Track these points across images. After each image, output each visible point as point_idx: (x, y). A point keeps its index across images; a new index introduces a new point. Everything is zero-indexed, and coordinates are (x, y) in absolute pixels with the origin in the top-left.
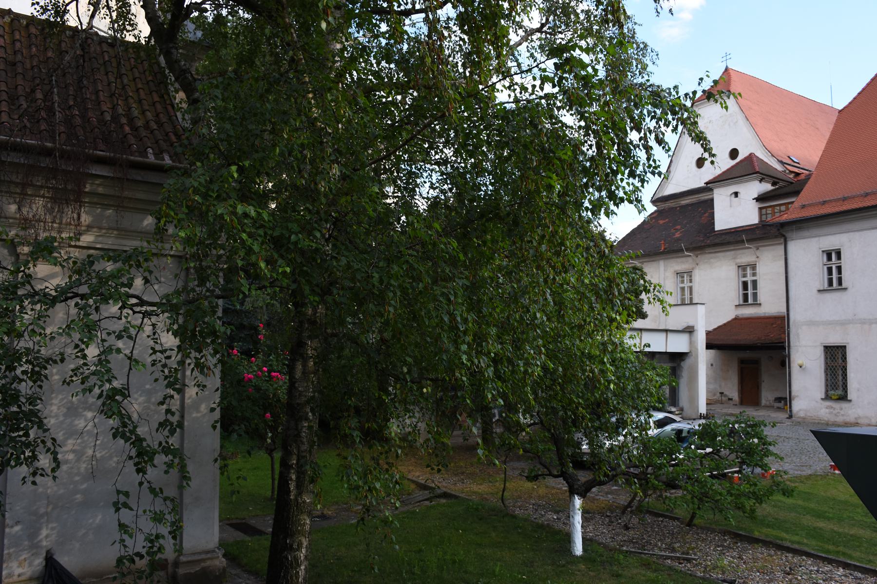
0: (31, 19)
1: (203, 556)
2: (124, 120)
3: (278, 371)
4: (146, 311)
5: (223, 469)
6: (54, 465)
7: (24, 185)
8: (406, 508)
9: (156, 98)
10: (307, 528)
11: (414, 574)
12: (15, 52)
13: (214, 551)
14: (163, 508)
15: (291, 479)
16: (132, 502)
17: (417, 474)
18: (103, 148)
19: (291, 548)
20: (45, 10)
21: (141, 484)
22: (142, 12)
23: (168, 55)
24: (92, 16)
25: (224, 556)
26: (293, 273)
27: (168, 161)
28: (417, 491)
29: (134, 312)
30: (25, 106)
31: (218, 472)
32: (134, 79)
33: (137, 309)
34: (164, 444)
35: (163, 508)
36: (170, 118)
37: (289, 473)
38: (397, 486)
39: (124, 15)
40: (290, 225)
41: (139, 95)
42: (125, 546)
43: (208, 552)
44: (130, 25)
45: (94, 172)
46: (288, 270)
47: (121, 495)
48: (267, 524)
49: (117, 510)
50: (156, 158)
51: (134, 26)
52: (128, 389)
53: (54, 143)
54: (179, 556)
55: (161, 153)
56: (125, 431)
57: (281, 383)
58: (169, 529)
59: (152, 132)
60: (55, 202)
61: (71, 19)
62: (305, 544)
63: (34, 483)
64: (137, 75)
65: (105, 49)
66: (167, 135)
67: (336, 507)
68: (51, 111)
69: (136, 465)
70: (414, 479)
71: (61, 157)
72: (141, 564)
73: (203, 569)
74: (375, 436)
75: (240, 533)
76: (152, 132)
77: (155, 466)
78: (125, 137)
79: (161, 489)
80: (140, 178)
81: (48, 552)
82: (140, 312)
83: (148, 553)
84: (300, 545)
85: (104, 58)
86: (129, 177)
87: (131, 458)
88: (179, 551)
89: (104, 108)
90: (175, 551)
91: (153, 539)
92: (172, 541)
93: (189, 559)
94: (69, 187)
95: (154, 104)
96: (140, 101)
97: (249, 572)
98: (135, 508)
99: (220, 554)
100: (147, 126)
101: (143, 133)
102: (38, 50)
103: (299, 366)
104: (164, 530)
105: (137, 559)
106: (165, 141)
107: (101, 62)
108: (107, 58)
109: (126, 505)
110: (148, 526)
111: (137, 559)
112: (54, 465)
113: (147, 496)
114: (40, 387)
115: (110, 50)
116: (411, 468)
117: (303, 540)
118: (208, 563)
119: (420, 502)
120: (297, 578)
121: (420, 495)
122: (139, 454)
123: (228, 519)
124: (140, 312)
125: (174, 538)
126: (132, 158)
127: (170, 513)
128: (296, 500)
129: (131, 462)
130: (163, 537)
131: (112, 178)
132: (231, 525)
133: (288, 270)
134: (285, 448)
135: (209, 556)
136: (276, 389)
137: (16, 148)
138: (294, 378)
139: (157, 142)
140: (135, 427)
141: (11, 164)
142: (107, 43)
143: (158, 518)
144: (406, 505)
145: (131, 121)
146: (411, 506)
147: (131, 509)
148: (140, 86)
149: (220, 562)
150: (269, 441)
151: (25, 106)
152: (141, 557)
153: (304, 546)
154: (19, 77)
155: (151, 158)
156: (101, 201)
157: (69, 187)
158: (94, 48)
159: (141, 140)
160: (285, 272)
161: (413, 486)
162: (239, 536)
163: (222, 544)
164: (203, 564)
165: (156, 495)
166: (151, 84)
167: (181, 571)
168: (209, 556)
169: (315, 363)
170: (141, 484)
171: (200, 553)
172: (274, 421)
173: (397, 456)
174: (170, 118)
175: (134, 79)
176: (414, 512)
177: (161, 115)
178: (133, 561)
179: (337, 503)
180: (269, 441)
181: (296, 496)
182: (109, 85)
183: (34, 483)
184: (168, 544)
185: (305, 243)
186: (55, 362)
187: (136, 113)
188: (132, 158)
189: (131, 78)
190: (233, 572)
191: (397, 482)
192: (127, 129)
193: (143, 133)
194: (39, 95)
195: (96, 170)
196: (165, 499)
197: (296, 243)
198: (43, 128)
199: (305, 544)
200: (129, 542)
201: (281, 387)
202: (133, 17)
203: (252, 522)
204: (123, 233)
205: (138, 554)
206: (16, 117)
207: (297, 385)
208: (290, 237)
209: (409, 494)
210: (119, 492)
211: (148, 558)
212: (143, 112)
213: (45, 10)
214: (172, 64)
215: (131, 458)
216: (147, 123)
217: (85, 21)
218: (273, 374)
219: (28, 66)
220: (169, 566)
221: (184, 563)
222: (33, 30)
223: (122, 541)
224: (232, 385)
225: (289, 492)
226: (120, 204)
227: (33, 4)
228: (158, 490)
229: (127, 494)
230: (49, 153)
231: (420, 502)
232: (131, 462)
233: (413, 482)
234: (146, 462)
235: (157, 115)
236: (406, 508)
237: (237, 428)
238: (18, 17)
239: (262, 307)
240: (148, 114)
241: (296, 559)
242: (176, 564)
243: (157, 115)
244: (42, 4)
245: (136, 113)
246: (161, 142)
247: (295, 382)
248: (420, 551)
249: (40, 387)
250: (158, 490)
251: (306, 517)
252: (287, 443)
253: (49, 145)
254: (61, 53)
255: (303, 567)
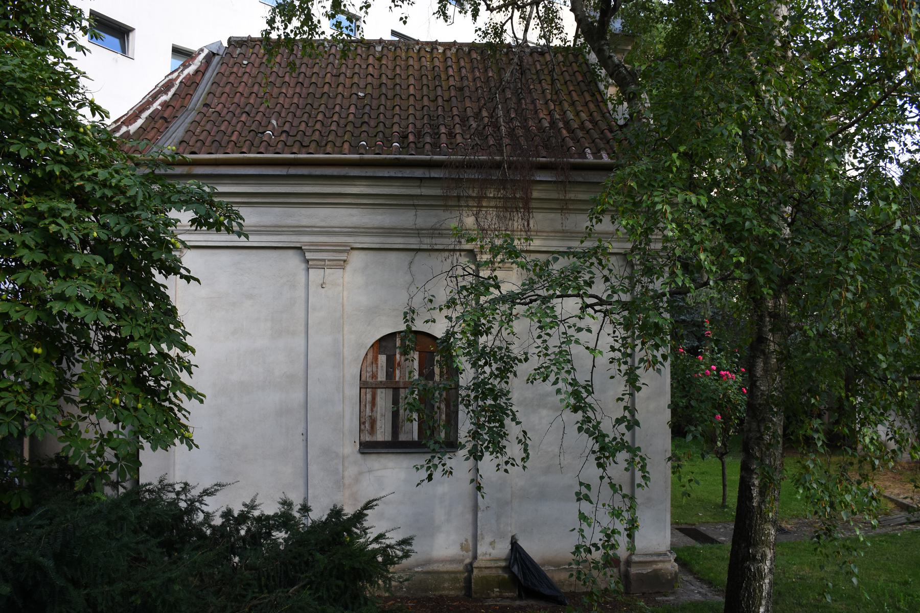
0: (473, 46)
1: (655, 558)
2: (561, 125)
3: (728, 370)
4: (607, 310)
5: (675, 470)
6: (524, 455)
7: (480, 198)
8: (883, 530)
9: (588, 98)
10: (772, 538)
11: (899, 609)
12: (462, 79)
13: (665, 554)
14: (621, 505)
15: (754, 485)
16: (593, 496)
17: (896, 491)
18: (544, 154)
19: (754, 559)
20: (486, 34)
21: (602, 478)
22: (572, 16)
23: (599, 53)
24: (526, 30)
25: (676, 560)
26: (747, 262)
27: (606, 159)
28: (897, 512)
29: (596, 311)
30: (474, 125)
31: (670, 471)
32: (566, 83)
33: (597, 308)
34: (619, 440)
35: (621, 505)
36: (603, 115)
37: (751, 478)
38: (874, 503)
39: (550, 21)
40: (743, 211)
41: (572, 97)
42: (583, 537)
43: (659, 555)
44: (557, 29)
45: (538, 179)
46: (742, 259)
47: (583, 487)
48: (724, 534)
49: (579, 500)
50: (595, 158)
51: (560, 29)
52: (591, 386)
53: (502, 155)
54: (631, 555)
55: (599, 151)
56: (590, 428)
57: (731, 382)
58: (625, 526)
59: (588, 132)
60: (507, 211)
61: (508, 37)
62: (769, 556)
63: (506, 471)
64: (568, 78)
65: (536, 59)
66: (602, 132)
67: (796, 520)
68: (498, 128)
69: (598, 459)
70: (892, 496)
71: (509, 168)
72: (597, 555)
73: (655, 571)
74: (840, 442)
75: (690, 539)
76: (588, 132)
77: (616, 463)
78: (563, 140)
79: (620, 486)
80: (581, 179)
81: (513, 537)
82: (600, 311)
83: (603, 545)
84: (764, 556)
85: (536, 68)
86: (570, 179)
87: (594, 452)
88: (632, 548)
89: (542, 116)
90: (628, 550)
91: (609, 534)
92: (627, 539)
93: (642, 559)
94: (518, 196)
95: (587, 103)
96: (573, 104)
97: (701, 580)
98: (594, 501)
99: (672, 557)
100: (582, 127)
101: (580, 134)
102: (541, 65)
103: (760, 364)
104: (620, 526)
105: (593, 549)
106: (601, 139)
107: (534, 71)
108: (539, 67)
109: (587, 498)
110: (606, 520)
111: (593, 549)
112: (524, 455)
113: (607, 491)
114: (507, 383)
115: (540, 59)
116: (888, 484)
117: (768, 551)
118: (660, 566)
119: (902, 524)
120: (761, 592)
121: (902, 516)
122: (602, 449)
123: (677, 523)
124: (600, 311)
125: (629, 536)
126: (572, 160)
127: (627, 511)
128: (759, 506)
129: (594, 456)
130: (619, 533)
131: (555, 182)
132: (681, 530)
133: (742, 259)
134: (746, 449)
135: (661, 558)
136: (726, 388)
137: (471, 165)
138: (755, 376)
139: (593, 141)
140: (599, 423)
141: (469, 180)
142: (538, 52)
143: (616, 514)
144: (883, 526)
145: (567, 124)
146: (890, 529)
147: (591, 503)
148: (571, 88)
149: (671, 566)
150: (719, 444)
151: (474, 125)
152: (598, 549)
153: (769, 558)
154: (467, 101)
155: (590, 158)
156: (549, 206)
157: (518, 196)
158: (527, 60)
159: (578, 141)
160: (739, 262)
161: (891, 505)
162: (689, 541)
163: (674, 548)
164: (654, 566)
165: (615, 492)
166: (582, 84)
167: (634, 570)
168: (661, 558)
169: (778, 360)
170: (602, 478)
171: (651, 555)
172: (724, 423)
173: (874, 468)
174: (603, 115)
175: (566, 83)
176: (894, 536)
177: (595, 114)
178: (590, 552)
179: (797, 517)
180: (719, 444)
181: (759, 504)
182: (543, 92)
183: (506, 471)
184: (622, 540)
185: (760, 230)
186: (520, 361)
187: (570, 115)
188: (572, 160)
189: (562, 82)
190: (685, 578)
191: (873, 498)
192: (564, 132)
193: (580, 134)
194: (485, 113)
195: (541, 176)
196: (624, 496)
197: (750, 230)
198: (491, 143)
199: (769, 556)
200: (587, 531)
201: (731, 386)
202: (559, 21)
203: (703, 529)
204: (569, 234)
205: (595, 545)
206: (468, 137)
207: (758, 384)
208: (744, 223)
209: (886, 514)
210: (581, 484)
211: (604, 551)
212: (577, 114)
213: (486, 34)
214: (605, 62)
215: (594, 452)
216: (582, 123)
217: (520, 35)
218: (723, 373)
219: (473, 89)
220: (622, 564)
221: (636, 563)
222: (474, 55)
223: (581, 530)
224: (683, 384)
225: (751, 498)
226: (564, 207)
227: (476, 31)
228: (617, 486)
229: (588, 487)
230: (498, 166)
231: (902, 524)
232: (594, 456)
233: (892, 500)
234: (607, 458)
235: (591, 115)
236: (883, 530)
237: (693, 428)
238: (462, 45)
239: (705, 303)
240: (582, 114)
241: (760, 571)
242: (628, 563)
243: (591, 115)
244: (483, 29)
245: (570, 115)
246: (598, 141)
247: (756, 381)
248: (906, 583)
249: (507, 383)
250: (617, 486)
251: (770, 527)
252: (748, 447)
253: (498, 158)
254: (500, 70)
255: (767, 581)
